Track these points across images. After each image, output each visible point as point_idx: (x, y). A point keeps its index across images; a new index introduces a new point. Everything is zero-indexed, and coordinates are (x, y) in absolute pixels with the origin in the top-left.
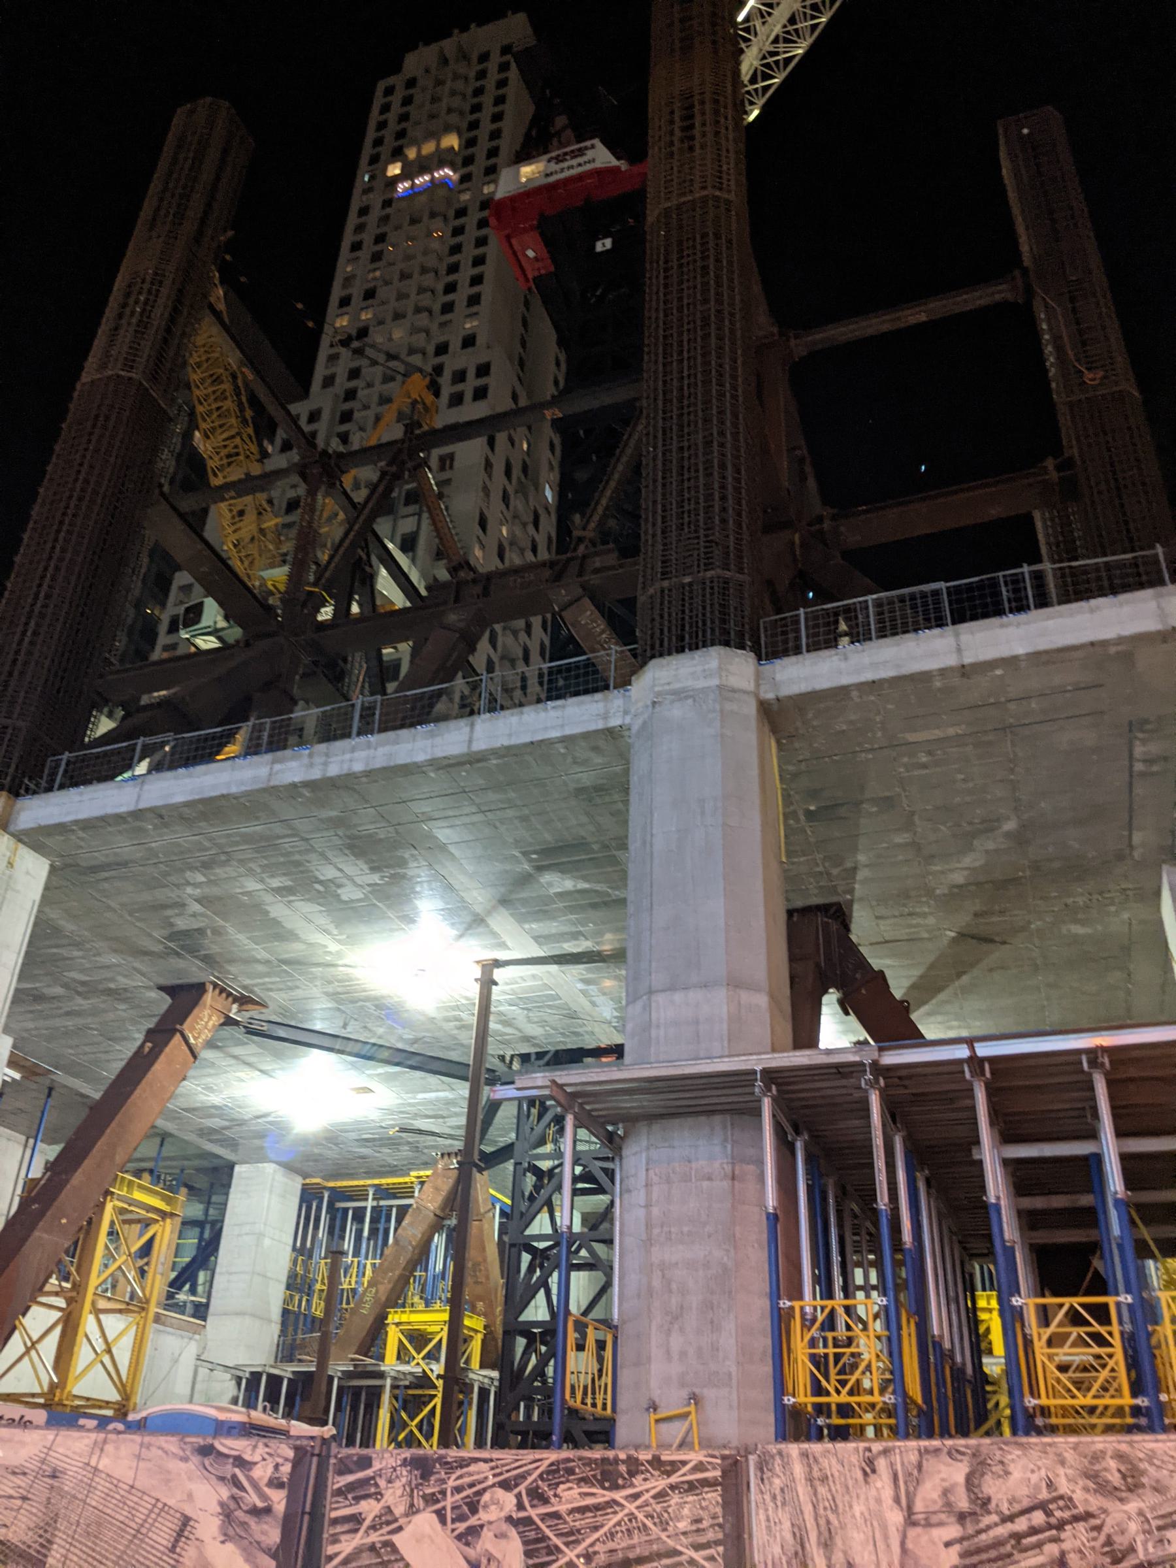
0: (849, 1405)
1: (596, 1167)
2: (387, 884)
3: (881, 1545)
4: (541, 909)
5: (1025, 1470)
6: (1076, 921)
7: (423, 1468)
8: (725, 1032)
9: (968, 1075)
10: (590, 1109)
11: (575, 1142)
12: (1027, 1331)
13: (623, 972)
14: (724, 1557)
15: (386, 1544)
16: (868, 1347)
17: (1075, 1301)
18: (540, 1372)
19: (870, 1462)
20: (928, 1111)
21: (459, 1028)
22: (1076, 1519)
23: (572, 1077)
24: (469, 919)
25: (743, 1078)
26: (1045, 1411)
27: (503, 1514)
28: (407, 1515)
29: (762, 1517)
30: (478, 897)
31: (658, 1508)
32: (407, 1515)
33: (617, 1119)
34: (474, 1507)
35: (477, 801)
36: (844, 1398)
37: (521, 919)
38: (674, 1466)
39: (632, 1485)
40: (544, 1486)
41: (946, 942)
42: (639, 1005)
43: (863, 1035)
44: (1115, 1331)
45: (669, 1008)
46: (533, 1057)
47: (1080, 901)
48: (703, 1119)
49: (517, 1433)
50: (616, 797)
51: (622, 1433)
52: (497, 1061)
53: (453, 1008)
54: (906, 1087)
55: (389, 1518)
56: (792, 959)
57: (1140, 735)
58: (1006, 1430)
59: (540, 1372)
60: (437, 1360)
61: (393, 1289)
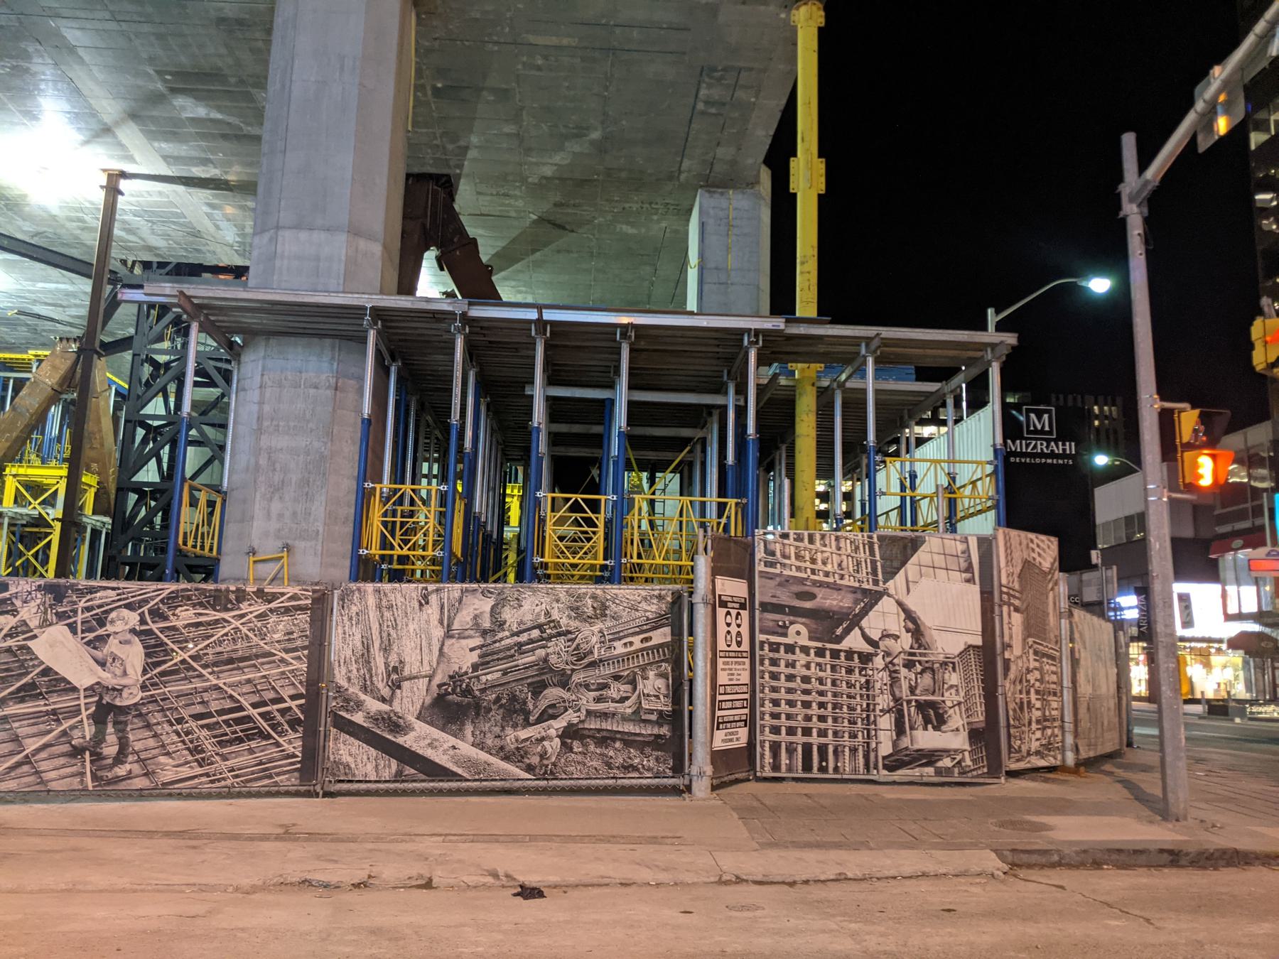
0: (408, 557)
1: (210, 366)
2: (8, 74)
3: (425, 649)
4: (167, 130)
5: (533, 604)
6: (628, 223)
7: (56, 592)
8: (342, 272)
9: (533, 333)
10: (216, 319)
11: (199, 342)
12: (542, 514)
13: (251, 204)
14: (308, 657)
15: (21, 648)
16: (427, 517)
17: (579, 497)
18: (149, 521)
19: (425, 597)
20: (498, 352)
21: (83, 229)
22: (559, 634)
23: (201, 290)
24: (95, 126)
25: (358, 311)
26: (545, 566)
27: (128, 627)
28: (41, 627)
29: (340, 631)
30: (109, 108)
31: (259, 624)
32: (41, 627)
33: (238, 331)
34: (102, 622)
35: (111, 8)
36: (405, 552)
37: (152, 136)
38: (274, 597)
39: (239, 608)
40: (164, 608)
41: (528, 224)
42: (267, 236)
43: (452, 287)
44: (600, 521)
45: (291, 243)
46: (155, 266)
47: (635, 207)
48: (316, 340)
49: (125, 564)
50: (258, 35)
51: (225, 569)
52: (118, 264)
53: (76, 210)
54: (484, 335)
55: (24, 628)
56: (405, 217)
57: (707, 80)
58: (511, 577)
59: (149, 521)
60: (53, 506)
61: (9, 448)
